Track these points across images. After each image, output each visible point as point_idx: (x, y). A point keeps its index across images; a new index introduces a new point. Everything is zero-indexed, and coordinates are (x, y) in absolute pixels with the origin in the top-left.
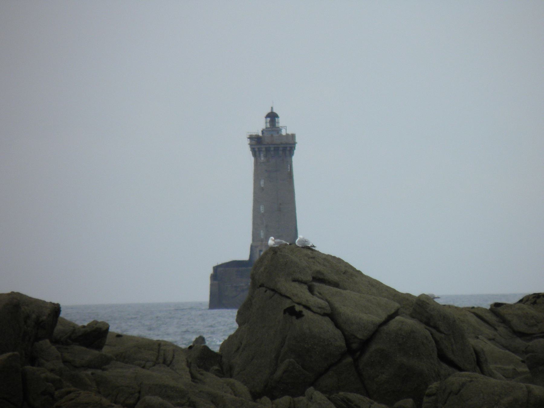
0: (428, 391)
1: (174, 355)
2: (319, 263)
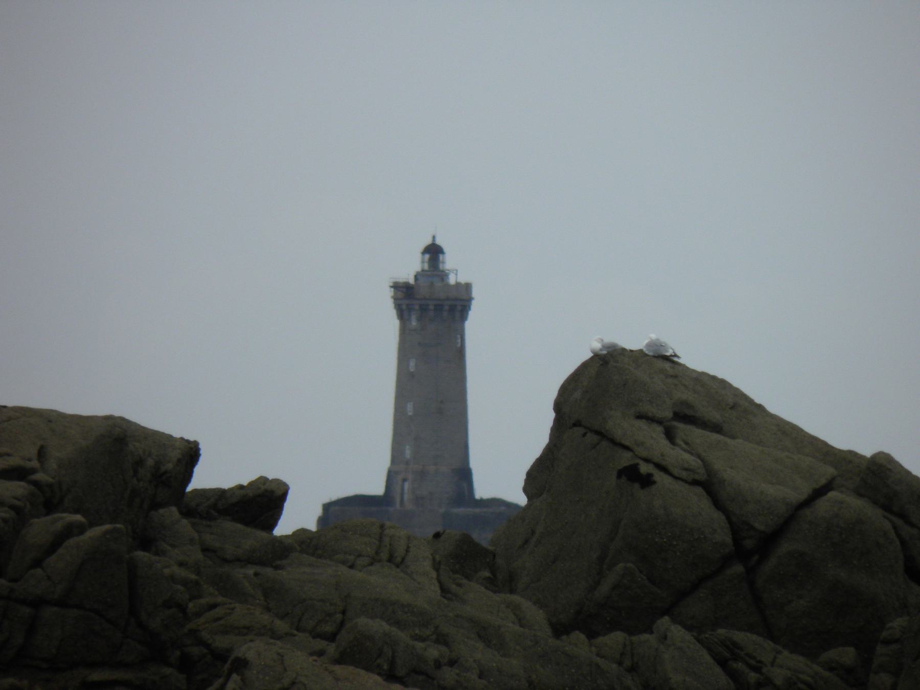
0: (885, 634)
1: (408, 547)
2: (685, 386)
